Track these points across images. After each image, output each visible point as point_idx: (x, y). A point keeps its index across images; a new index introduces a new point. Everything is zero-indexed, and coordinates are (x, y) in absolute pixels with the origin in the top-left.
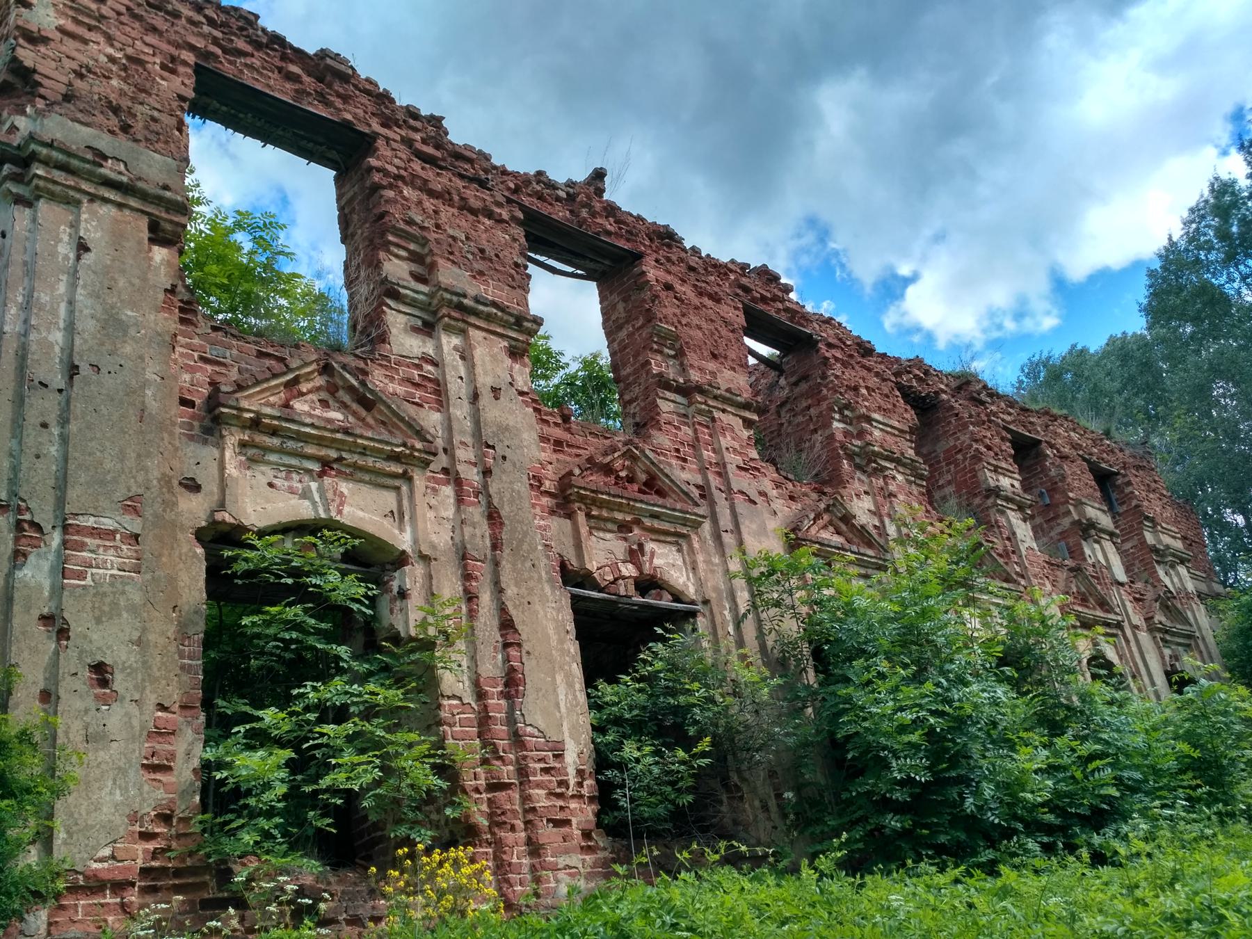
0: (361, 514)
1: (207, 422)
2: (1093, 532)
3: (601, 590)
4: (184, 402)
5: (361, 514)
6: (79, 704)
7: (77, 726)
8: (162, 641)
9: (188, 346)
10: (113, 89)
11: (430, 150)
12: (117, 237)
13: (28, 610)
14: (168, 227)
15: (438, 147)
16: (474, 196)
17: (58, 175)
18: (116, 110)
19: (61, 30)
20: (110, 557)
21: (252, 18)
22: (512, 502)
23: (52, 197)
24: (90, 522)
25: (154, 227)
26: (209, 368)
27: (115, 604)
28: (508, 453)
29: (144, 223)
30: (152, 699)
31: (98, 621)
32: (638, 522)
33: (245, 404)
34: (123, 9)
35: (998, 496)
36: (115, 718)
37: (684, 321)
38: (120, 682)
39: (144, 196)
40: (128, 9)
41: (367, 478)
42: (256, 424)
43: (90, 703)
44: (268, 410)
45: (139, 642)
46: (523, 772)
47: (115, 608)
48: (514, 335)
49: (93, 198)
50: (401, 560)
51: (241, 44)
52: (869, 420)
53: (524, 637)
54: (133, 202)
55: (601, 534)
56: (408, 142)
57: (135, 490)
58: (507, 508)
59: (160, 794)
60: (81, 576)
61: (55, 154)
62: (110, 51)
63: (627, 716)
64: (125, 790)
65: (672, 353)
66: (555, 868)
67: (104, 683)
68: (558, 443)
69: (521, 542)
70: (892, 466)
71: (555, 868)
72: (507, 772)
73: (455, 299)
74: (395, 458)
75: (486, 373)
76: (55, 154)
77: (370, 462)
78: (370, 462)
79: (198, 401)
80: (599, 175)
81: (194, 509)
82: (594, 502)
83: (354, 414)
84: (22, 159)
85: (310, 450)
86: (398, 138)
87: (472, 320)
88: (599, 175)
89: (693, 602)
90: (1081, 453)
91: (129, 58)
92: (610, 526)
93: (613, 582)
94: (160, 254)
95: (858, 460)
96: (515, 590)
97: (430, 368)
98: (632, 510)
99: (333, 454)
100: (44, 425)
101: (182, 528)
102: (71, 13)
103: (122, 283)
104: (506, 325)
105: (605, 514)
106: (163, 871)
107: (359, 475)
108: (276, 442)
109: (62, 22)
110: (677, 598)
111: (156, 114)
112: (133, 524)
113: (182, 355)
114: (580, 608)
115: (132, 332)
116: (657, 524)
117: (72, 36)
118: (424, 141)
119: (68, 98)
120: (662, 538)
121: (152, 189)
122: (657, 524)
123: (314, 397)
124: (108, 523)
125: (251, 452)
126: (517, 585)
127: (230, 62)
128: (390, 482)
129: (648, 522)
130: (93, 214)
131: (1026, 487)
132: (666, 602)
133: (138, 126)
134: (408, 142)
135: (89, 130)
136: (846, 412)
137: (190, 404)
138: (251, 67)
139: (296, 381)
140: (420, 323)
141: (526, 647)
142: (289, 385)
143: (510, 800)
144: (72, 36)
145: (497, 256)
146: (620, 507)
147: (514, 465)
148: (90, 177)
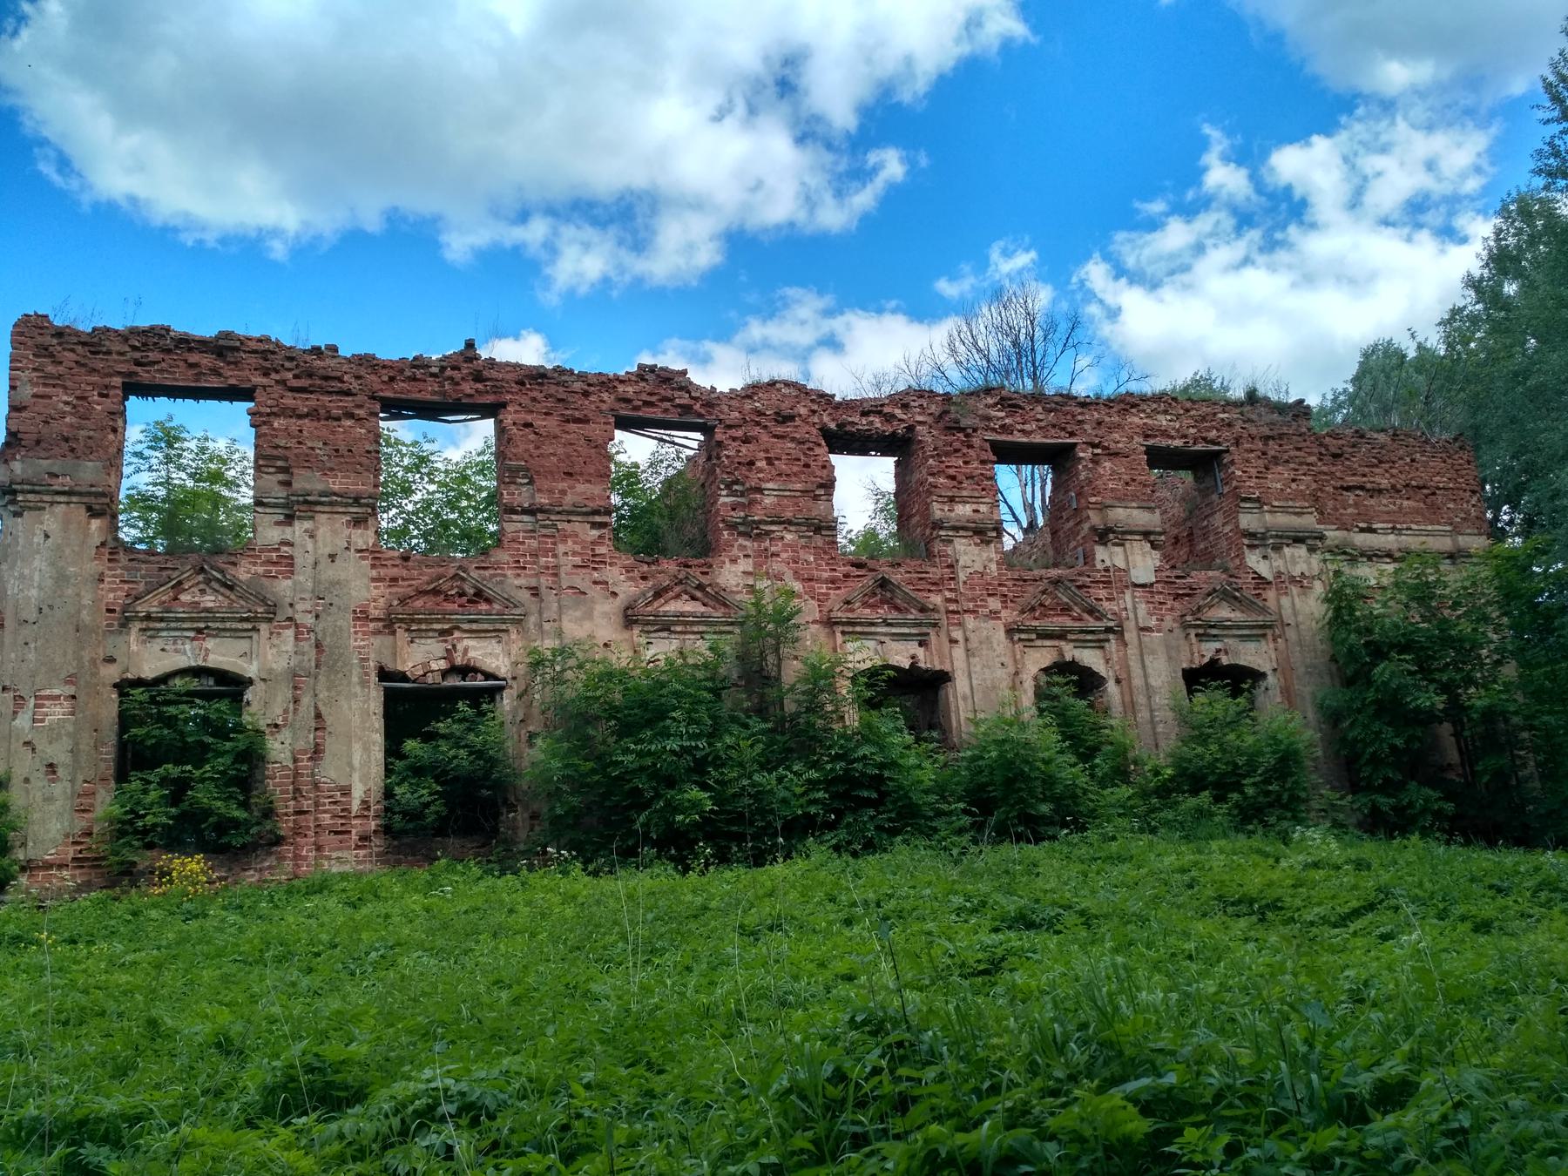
0: (221, 659)
1: (123, 621)
2: (1111, 536)
3: (414, 682)
4: (109, 611)
5: (221, 659)
6: (41, 784)
7: (39, 794)
8: (87, 748)
9: (113, 576)
10: (67, 425)
11: (304, 382)
12: (66, 523)
13: (17, 741)
14: (97, 507)
15: (310, 376)
16: (336, 405)
17: (30, 497)
18: (66, 440)
19: (35, 396)
20: (58, 709)
21: (163, 332)
22: (332, 635)
23: (30, 509)
24: (47, 692)
25: (89, 509)
26: (126, 587)
27: (59, 734)
28: (336, 601)
29: (83, 510)
30: (80, 778)
31: (50, 743)
32: (458, 628)
33: (139, 609)
34: (73, 365)
35: (941, 528)
36: (58, 789)
37: (537, 452)
38: (61, 772)
39: (80, 494)
40: (77, 362)
42: (148, 617)
43: (46, 783)
44: (154, 609)
45: (72, 751)
46: (317, 804)
47: (59, 736)
48: (354, 510)
49: (52, 503)
50: (250, 682)
51: (153, 356)
52: (760, 490)
53: (328, 723)
54: (74, 499)
55: (423, 641)
56: (283, 382)
57: (72, 671)
58: (328, 640)
59: (84, 823)
60: (42, 721)
61: (25, 487)
62: (65, 398)
63: (170, 766)
64: (62, 823)
65: (526, 481)
66: (329, 858)
67: (54, 773)
68: (394, 580)
69: (336, 661)
70: (780, 527)
71: (329, 858)
72: (306, 804)
73: (301, 499)
74: (247, 620)
75: (325, 546)
76: (25, 487)
77: (228, 625)
78: (228, 625)
79: (118, 609)
80: (470, 345)
81: (112, 673)
82: (413, 621)
83: (222, 594)
84: (9, 491)
86: (273, 383)
87: (319, 508)
88: (470, 345)
89: (504, 679)
91: (77, 398)
93: (424, 675)
94: (95, 524)
95: (741, 529)
96: (326, 694)
97: (286, 549)
99: (202, 625)
100: (26, 644)
101: (104, 685)
102: (41, 381)
103: (68, 551)
104: (347, 505)
105: (423, 627)
106: (86, 859)
107: (223, 634)
108: (163, 625)
109: (35, 390)
110: (489, 676)
111: (92, 433)
112: (70, 690)
113: (109, 583)
114: (391, 698)
115: (72, 581)
116: (474, 626)
117: (42, 397)
118: (295, 377)
119: (38, 442)
121: (84, 489)
122: (474, 626)
123: (195, 590)
124: (57, 692)
125: (149, 633)
126: (329, 689)
127: (148, 372)
128: (245, 634)
129: (465, 626)
130: (52, 513)
132: (480, 682)
133: (80, 447)
134: (283, 382)
135: (49, 461)
136: (735, 487)
137: (112, 611)
138: (161, 371)
139: (180, 583)
140: (282, 517)
141: (329, 729)
143: (306, 820)
144: (42, 397)
145: (350, 451)
146: (438, 621)
147: (339, 608)
148: (48, 493)
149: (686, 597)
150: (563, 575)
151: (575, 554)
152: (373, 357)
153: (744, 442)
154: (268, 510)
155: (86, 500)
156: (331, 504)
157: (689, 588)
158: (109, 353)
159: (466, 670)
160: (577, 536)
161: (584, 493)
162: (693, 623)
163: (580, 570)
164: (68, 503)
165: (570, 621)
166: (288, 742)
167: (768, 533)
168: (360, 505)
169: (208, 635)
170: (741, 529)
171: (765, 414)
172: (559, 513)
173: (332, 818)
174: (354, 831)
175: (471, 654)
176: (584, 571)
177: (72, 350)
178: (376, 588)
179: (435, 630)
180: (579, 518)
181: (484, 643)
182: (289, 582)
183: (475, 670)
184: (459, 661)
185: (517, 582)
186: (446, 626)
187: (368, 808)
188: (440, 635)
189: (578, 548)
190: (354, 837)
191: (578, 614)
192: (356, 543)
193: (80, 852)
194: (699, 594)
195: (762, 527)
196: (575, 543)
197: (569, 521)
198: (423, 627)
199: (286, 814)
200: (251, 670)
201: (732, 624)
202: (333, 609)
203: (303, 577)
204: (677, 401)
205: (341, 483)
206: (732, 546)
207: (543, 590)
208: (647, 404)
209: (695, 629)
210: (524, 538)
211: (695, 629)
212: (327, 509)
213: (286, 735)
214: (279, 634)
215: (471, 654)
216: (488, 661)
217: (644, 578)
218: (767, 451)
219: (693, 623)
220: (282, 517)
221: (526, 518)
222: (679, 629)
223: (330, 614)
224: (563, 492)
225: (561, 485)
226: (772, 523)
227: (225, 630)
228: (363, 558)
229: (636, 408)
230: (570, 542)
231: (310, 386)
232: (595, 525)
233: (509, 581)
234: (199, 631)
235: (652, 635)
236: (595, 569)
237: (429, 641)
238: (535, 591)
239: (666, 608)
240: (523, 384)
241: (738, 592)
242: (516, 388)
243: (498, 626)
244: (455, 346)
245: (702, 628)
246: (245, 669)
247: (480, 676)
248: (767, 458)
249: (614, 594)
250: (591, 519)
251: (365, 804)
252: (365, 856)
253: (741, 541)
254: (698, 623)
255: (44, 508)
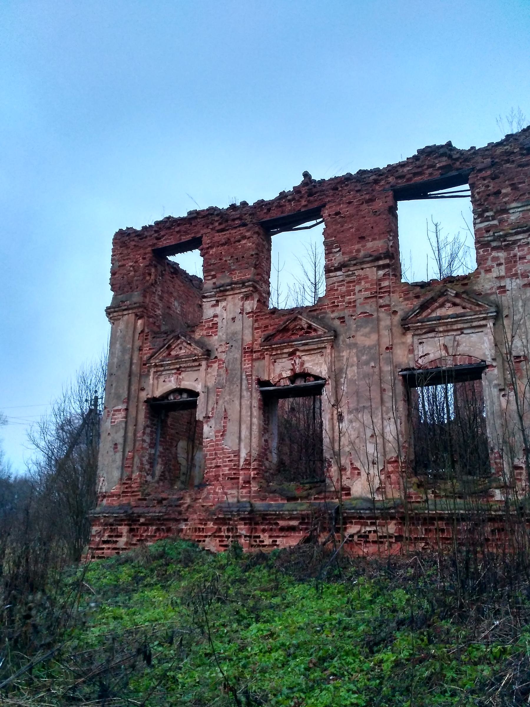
3: (275, 385)
32: (298, 350)
41: (189, 369)
48: (243, 290)
54: (130, 312)
58: (230, 366)
77: (188, 364)
78: (188, 364)
80: (306, 175)
82: (273, 349)
85: (172, 367)
87: (228, 293)
88: (306, 175)
90: (425, 167)
92: (284, 356)
93: (279, 381)
95: (494, 244)
98: (292, 346)
99: (178, 366)
104: (240, 288)
105: (279, 352)
108: (163, 368)
109: (120, 263)
110: (317, 378)
116: (306, 348)
120: (312, 352)
122: (306, 348)
126: (230, 395)
129: (301, 348)
130: (123, 320)
131: (255, 492)
132: (311, 382)
138: (165, 240)
141: (229, 418)
142: (167, 348)
146: (286, 347)
149: (449, 305)
150: (358, 305)
151: (366, 290)
152: (263, 201)
153: (493, 179)
154: (209, 300)
155: (134, 311)
156: (232, 289)
157: (450, 298)
158: (146, 237)
159: (305, 375)
160: (367, 278)
161: (372, 248)
162: (452, 323)
163: (368, 301)
164: (129, 314)
165: (362, 335)
166: (213, 427)
167: (515, 242)
168: (247, 287)
169: (182, 371)
170: (494, 244)
171: (513, 153)
172: (355, 265)
173: (229, 470)
174: (241, 478)
175: (307, 365)
176: (372, 300)
177: (133, 240)
178: (257, 333)
179: (286, 353)
180: (368, 265)
181: (313, 357)
182: (216, 337)
183: (309, 375)
184: (298, 370)
185: (332, 316)
186: (291, 350)
187: (249, 464)
188: (290, 355)
189: (368, 285)
190: (241, 481)
191: (367, 330)
192: (246, 309)
193: (127, 488)
194: (458, 301)
195: (508, 239)
196: (366, 282)
197: (362, 269)
198: (279, 352)
199: (211, 468)
200: (199, 388)
201: (484, 319)
202: (233, 348)
203: (221, 334)
204: (438, 165)
205: (238, 277)
206: (487, 259)
207: (347, 318)
208: (415, 174)
209: (455, 327)
210: (338, 286)
211: (455, 327)
212: (231, 293)
213: (212, 422)
214: (212, 366)
215: (307, 365)
216: (315, 368)
217: (417, 297)
218: (512, 179)
219: (452, 323)
220: (214, 302)
221: (339, 273)
222: (441, 329)
223: (231, 352)
224: (358, 251)
225: (357, 247)
226: (517, 233)
227: (188, 367)
228: (249, 317)
229: (409, 180)
230: (363, 283)
231: (226, 227)
232: (379, 268)
233: (328, 316)
234: (178, 369)
235: (424, 336)
236: (381, 297)
237: (284, 360)
238: (342, 319)
239: (434, 315)
240: (337, 189)
241: (492, 294)
242: (331, 192)
243: (319, 346)
244: (299, 180)
245: (459, 326)
246: (195, 387)
247: (312, 379)
248: (511, 185)
249: (395, 312)
250: (376, 264)
251: (248, 462)
252: (246, 493)
253: (494, 254)
254: (456, 322)
255: (120, 319)
